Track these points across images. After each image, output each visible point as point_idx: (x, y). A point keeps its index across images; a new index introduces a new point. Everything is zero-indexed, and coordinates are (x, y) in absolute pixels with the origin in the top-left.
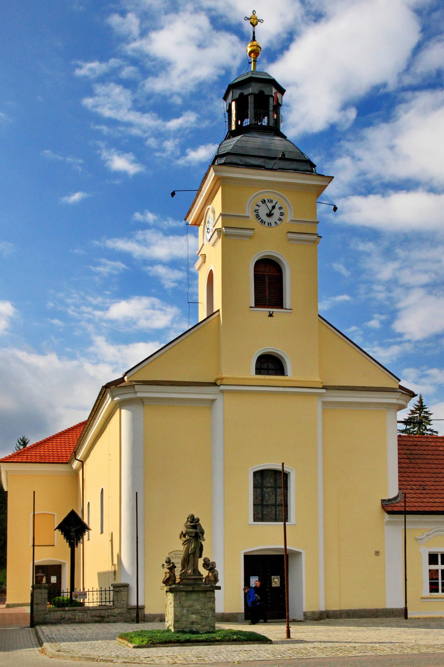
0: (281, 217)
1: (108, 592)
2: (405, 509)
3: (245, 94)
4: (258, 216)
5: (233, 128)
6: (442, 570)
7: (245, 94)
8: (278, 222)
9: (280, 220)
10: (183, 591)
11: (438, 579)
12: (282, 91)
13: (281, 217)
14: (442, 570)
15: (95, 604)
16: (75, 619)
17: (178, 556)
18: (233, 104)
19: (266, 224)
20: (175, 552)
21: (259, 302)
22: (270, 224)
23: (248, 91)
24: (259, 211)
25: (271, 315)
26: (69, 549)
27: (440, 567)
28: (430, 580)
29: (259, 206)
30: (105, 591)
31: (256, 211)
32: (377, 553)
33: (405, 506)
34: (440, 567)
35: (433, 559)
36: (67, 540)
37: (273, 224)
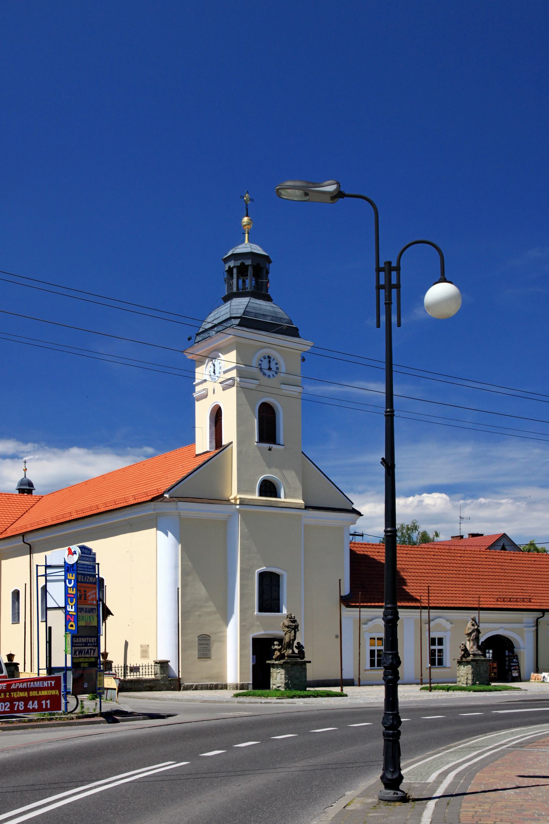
3: (246, 264)
5: (235, 290)
18: (235, 271)
21: (262, 439)
22: (269, 376)
23: (248, 262)
25: (270, 449)
31: (260, 365)
33: (429, 603)
37: (271, 376)
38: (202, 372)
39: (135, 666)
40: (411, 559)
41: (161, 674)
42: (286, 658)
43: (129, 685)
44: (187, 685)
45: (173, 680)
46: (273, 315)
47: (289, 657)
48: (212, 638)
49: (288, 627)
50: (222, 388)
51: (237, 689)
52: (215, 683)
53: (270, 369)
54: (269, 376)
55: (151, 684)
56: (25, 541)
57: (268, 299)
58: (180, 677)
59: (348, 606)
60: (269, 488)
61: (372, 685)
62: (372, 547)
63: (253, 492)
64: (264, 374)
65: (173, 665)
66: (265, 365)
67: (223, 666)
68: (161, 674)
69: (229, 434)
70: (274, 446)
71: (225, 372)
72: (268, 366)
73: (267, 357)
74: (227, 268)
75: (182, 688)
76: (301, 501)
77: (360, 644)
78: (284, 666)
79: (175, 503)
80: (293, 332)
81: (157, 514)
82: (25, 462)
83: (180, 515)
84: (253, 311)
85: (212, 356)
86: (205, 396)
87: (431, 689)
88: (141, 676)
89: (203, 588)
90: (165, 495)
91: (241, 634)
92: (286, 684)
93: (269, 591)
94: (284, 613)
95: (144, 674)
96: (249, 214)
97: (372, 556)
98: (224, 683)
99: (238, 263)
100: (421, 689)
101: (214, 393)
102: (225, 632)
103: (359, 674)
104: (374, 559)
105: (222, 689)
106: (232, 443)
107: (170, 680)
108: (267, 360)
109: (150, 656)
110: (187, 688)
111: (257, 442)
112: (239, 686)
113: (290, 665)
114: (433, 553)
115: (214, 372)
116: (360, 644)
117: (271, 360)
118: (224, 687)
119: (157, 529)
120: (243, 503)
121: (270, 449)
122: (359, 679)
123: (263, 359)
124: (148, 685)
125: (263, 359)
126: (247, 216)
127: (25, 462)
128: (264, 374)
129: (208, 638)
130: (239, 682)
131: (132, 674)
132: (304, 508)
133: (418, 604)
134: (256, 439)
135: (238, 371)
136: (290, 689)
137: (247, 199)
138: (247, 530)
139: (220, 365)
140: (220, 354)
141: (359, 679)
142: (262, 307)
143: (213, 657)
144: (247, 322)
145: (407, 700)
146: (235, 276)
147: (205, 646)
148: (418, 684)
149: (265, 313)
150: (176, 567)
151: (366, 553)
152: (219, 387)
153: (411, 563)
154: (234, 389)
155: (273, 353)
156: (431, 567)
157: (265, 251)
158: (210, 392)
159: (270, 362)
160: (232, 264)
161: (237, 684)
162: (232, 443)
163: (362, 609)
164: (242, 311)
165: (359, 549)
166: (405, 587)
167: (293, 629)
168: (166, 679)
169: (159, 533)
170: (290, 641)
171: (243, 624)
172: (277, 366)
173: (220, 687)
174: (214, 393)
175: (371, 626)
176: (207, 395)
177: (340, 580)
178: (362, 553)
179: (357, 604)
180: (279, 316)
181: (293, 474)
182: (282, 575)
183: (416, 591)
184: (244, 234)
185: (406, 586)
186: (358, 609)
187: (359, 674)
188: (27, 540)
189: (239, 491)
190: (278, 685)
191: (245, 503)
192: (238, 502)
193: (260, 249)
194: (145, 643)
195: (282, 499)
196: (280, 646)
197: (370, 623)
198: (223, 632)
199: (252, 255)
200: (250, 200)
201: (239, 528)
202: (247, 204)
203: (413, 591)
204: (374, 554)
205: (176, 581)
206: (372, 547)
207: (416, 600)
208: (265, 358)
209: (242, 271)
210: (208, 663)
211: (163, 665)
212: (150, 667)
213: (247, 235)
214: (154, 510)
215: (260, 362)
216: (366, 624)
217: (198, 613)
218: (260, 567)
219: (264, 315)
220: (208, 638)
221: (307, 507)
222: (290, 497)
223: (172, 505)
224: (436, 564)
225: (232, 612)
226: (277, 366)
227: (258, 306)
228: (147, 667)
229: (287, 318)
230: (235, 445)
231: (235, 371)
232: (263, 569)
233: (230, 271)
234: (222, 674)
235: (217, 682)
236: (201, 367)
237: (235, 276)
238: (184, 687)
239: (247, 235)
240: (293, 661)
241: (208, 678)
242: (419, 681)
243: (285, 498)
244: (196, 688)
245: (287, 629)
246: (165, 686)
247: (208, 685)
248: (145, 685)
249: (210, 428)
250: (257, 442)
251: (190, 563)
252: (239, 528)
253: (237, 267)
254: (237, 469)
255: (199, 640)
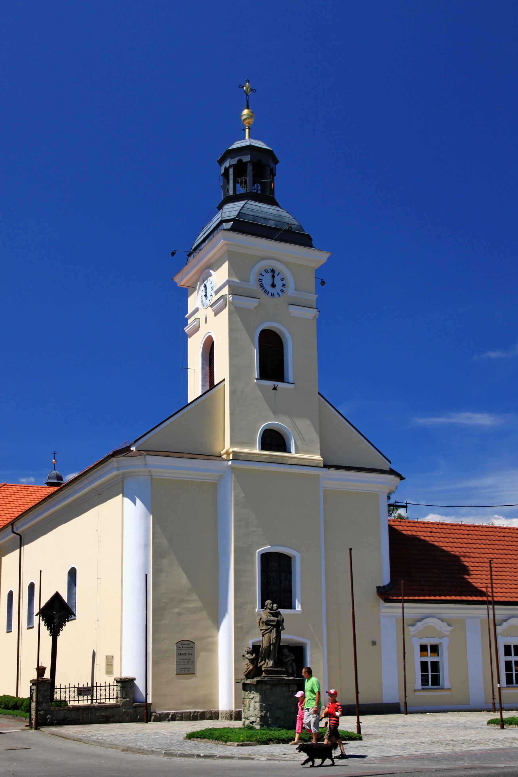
0: (283, 289)
1: (112, 688)
2: (493, 599)
3: (244, 161)
4: (262, 285)
5: (231, 193)
6: (515, 662)
7: (244, 161)
8: (280, 293)
9: (282, 291)
10: (269, 684)
11: (512, 671)
12: (276, 162)
13: (283, 289)
14: (515, 662)
15: (112, 702)
16: (79, 720)
17: (185, 646)
18: (231, 171)
19: (270, 294)
20: (182, 642)
21: (264, 375)
22: (273, 295)
23: (246, 159)
24: (263, 280)
26: (51, 638)
27: (513, 658)
28: (422, 672)
29: (263, 275)
30: (65, 688)
31: (260, 280)
32: (374, 643)
34: (513, 658)
35: (507, 650)
36: (48, 627)
37: (276, 294)
38: (194, 301)
39: (86, 686)
40: (474, 541)
41: (122, 697)
42: (264, 674)
43: (74, 715)
44: (160, 714)
45: (140, 706)
46: (277, 219)
47: (268, 672)
48: (197, 646)
49: (267, 623)
50: (213, 313)
51: (231, 719)
52: (201, 710)
53: (273, 285)
54: (273, 295)
55: (108, 713)
56: (14, 531)
57: (273, 202)
58: (150, 701)
59: (387, 600)
60: (273, 440)
61: (424, 712)
62: (423, 526)
63: (252, 444)
64: (266, 292)
65: (140, 683)
66: (267, 280)
67: (213, 686)
68: (122, 697)
69: (222, 370)
70: (280, 385)
71: (217, 292)
72: (271, 282)
73: (269, 271)
74: (223, 171)
75: (153, 718)
76: (318, 457)
77: (404, 653)
78: (259, 687)
79: (142, 457)
80: (302, 239)
81: (123, 474)
82: (55, 454)
83: (151, 475)
84: (250, 213)
85: (203, 276)
86: (197, 329)
87: (502, 723)
88: (103, 701)
89: (184, 575)
90: (132, 449)
91: (236, 640)
92: (262, 718)
93: (277, 579)
94: (297, 609)
95: (107, 697)
96: (249, 107)
97: (422, 537)
98: (214, 710)
99: (234, 161)
100: (489, 723)
101: (206, 322)
102: (216, 636)
103: (406, 697)
104: (425, 541)
105: (211, 718)
106: (224, 380)
107: (135, 707)
108: (270, 274)
109: (114, 672)
110: (161, 718)
111: (257, 379)
112: (233, 715)
113: (269, 687)
114: (502, 534)
115: (205, 296)
116: (404, 653)
117: (276, 275)
118: (215, 716)
119: (123, 496)
120: (237, 457)
121: (275, 389)
122: (406, 703)
123: (264, 273)
124: (103, 714)
125: (264, 273)
126: (248, 108)
127: (55, 454)
128: (266, 292)
129: (191, 645)
130: (233, 709)
131: (81, 698)
132: (322, 466)
133: (485, 599)
134: (256, 375)
135: (230, 287)
136: (269, 726)
137: (247, 89)
138: (243, 495)
139: (212, 285)
140: (211, 271)
141: (406, 703)
142: (263, 209)
143: (198, 673)
144: (242, 226)
145: (457, 749)
146: (231, 177)
147: (187, 657)
148: (489, 711)
149: (267, 216)
150: (146, 546)
151: (414, 533)
152: (210, 312)
153: (474, 546)
154: (226, 311)
155: (279, 267)
156: (500, 551)
157: (270, 147)
158: (202, 321)
159: (273, 276)
160: (227, 164)
161: (231, 712)
162: (224, 380)
163: (406, 605)
164: (236, 213)
165: (406, 528)
166: (467, 577)
167: (274, 626)
168: (130, 706)
169: (126, 499)
170: (269, 646)
171: (239, 625)
172: (283, 282)
173: (208, 716)
174: (206, 322)
175: (420, 629)
176: (199, 327)
177: (351, 549)
178: (409, 533)
179: (400, 598)
180: (286, 221)
181: (307, 422)
182: (295, 557)
183: (481, 581)
184: (244, 130)
185: (469, 574)
186: (400, 605)
187: (406, 697)
188: (17, 529)
189: (233, 443)
190: (252, 719)
191: (241, 458)
192: (231, 457)
193: (263, 144)
194: (110, 654)
195: (293, 454)
196: (254, 655)
197: (419, 624)
198: (209, 637)
199: (250, 148)
200: (252, 90)
201: (232, 493)
202: (247, 95)
203: (476, 581)
204: (425, 534)
205: (146, 565)
206: (423, 526)
207: (482, 594)
208: (266, 271)
209: (240, 169)
210: (192, 681)
211: (126, 684)
212: (107, 688)
213: (247, 130)
214: (118, 468)
215: (261, 277)
216: (413, 625)
217: (177, 610)
218: (265, 545)
219: (265, 219)
220: (191, 645)
221: (326, 466)
222: (304, 451)
223: (138, 461)
224: (507, 548)
225: (225, 610)
226: (283, 282)
227: (258, 208)
228: (103, 688)
229: (296, 223)
230: (227, 383)
231: (227, 288)
232: (267, 548)
233: (226, 174)
234: (212, 699)
235: (204, 708)
236: (193, 294)
237: (231, 177)
238: (155, 716)
239: (247, 130)
240: (275, 678)
241: (193, 703)
242: (491, 706)
243: (297, 452)
244: (174, 718)
245: (265, 627)
246: (128, 715)
247: (190, 713)
248: (98, 714)
249: (203, 368)
250: (257, 379)
251: (165, 541)
252: (232, 493)
253: (234, 166)
254: (230, 413)
255: (178, 648)
